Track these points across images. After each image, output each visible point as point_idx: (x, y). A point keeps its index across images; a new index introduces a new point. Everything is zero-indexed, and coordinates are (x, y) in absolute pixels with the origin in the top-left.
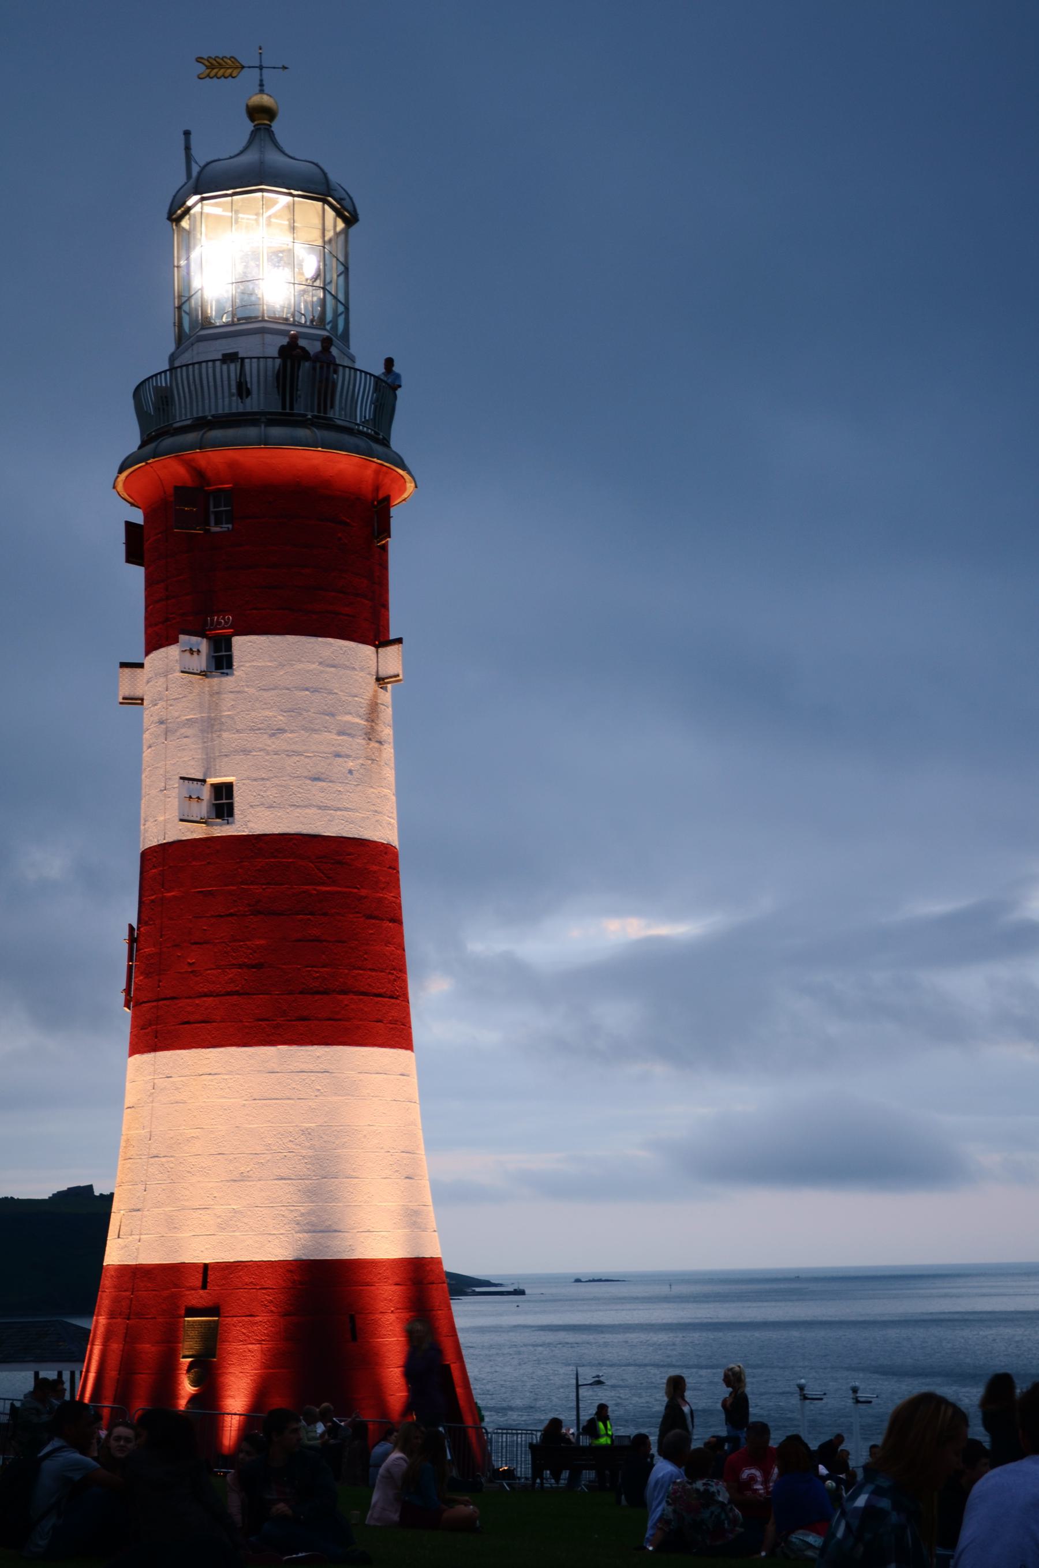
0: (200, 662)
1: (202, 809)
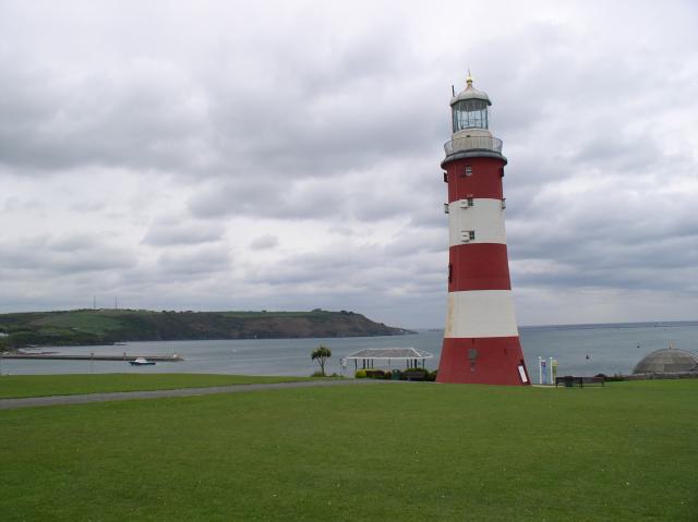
0: (466, 205)
1: (468, 238)
